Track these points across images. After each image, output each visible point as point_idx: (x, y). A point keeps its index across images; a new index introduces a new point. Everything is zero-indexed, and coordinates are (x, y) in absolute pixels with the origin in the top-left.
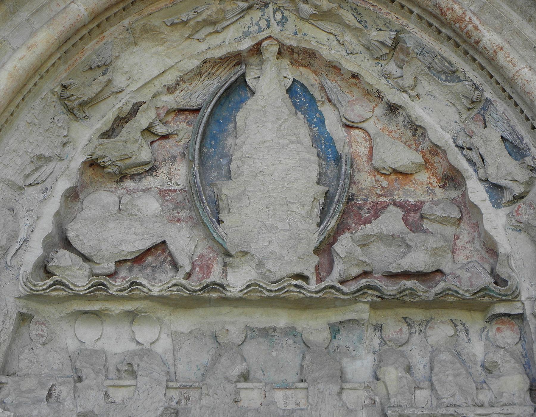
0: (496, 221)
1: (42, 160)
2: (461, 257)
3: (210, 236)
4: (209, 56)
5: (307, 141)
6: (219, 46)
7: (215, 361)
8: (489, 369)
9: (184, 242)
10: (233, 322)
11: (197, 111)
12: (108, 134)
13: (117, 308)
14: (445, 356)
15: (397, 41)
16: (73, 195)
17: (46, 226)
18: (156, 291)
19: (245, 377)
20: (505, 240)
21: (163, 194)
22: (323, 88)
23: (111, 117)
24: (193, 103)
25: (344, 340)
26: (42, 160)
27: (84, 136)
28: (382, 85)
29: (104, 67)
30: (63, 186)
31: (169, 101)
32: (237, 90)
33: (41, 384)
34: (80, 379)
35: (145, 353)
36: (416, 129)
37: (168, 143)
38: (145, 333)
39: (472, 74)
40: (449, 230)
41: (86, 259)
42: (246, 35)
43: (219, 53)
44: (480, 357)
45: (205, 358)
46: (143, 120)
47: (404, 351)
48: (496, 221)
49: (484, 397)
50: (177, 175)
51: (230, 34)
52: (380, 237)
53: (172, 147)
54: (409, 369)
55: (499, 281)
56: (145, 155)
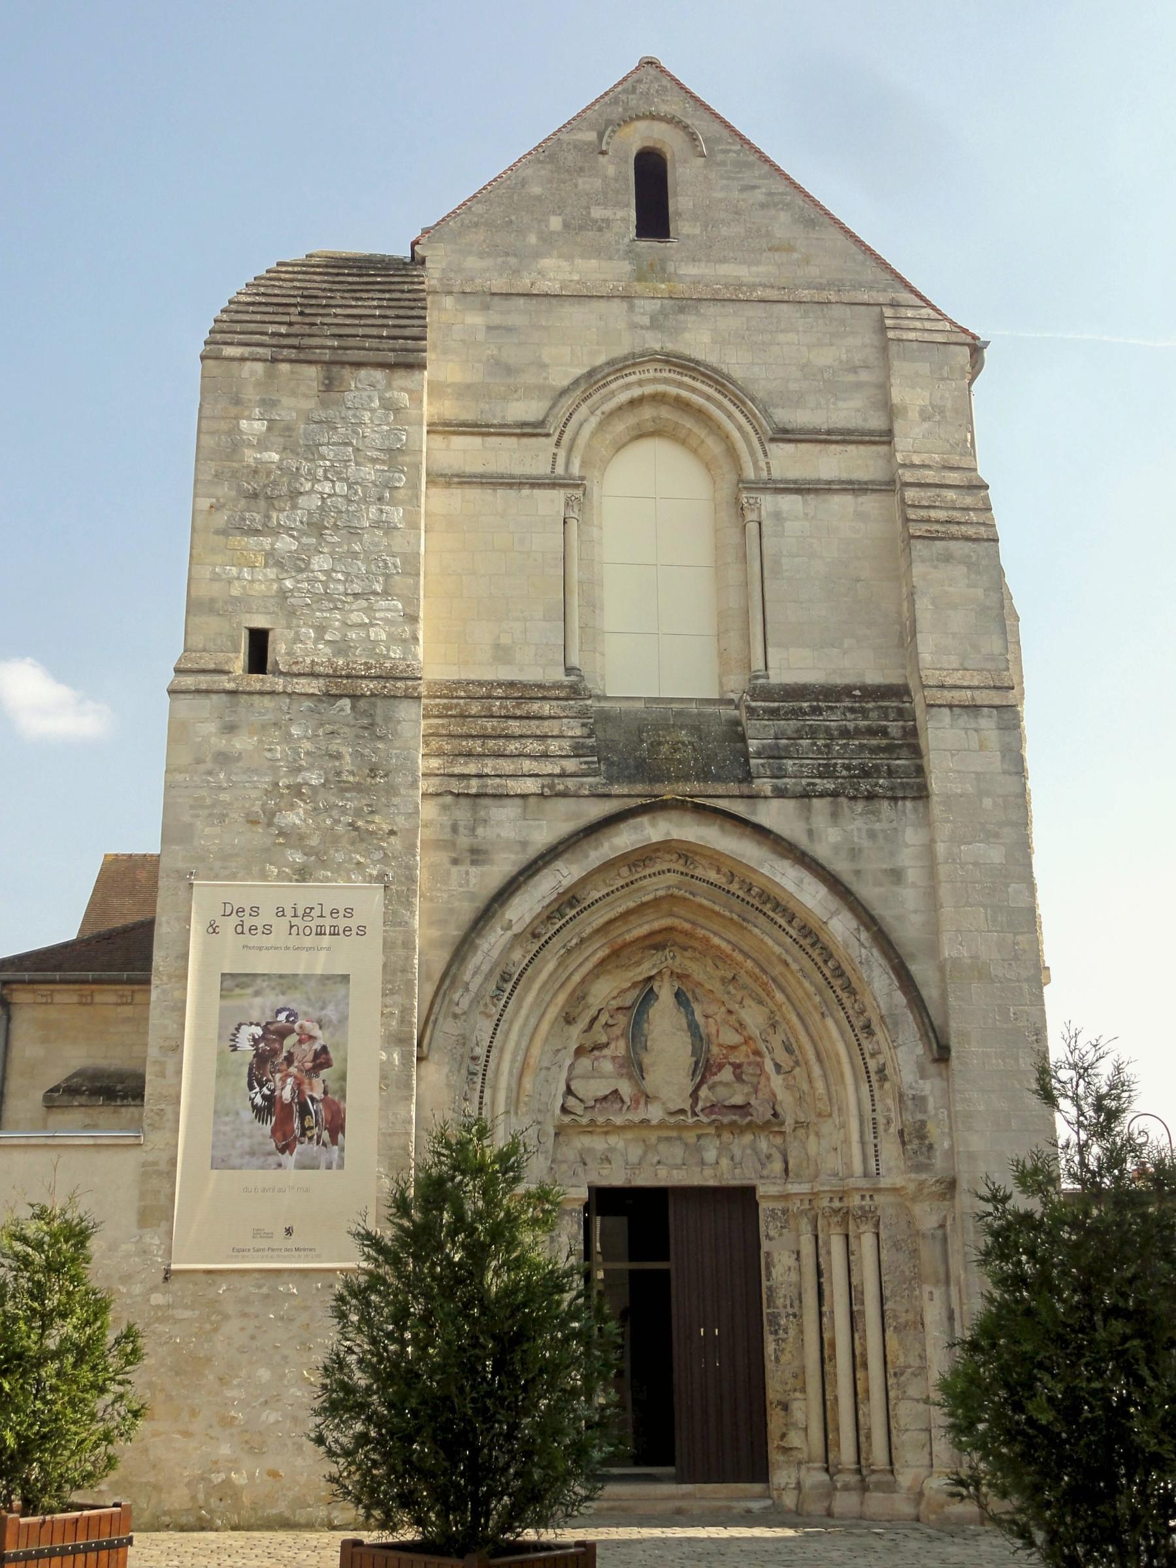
0: (777, 1082)
1: (558, 1051)
2: (760, 1094)
3: (637, 1084)
4: (635, 979)
5: (685, 1026)
6: (640, 974)
7: (645, 1153)
8: (769, 1157)
9: (626, 1089)
10: (653, 1137)
11: (629, 1008)
12: (585, 1031)
13: (599, 1130)
14: (749, 1151)
15: (734, 978)
16: (572, 1065)
17: (562, 1087)
18: (618, 1123)
19: (659, 1162)
20: (782, 1095)
21: (614, 1058)
22: (693, 992)
23: (588, 1020)
24: (628, 1003)
25: (702, 1142)
26: (558, 1051)
27: (575, 1032)
28: (726, 998)
29: (584, 998)
30: (568, 1062)
31: (615, 1004)
32: (648, 996)
33: (570, 1168)
34: (585, 1164)
35: (612, 1150)
36: (741, 1026)
37: (615, 1028)
38: (613, 1140)
39: (770, 1004)
40: (755, 1080)
41: (581, 1100)
42: (654, 966)
43: (641, 978)
44: (765, 1151)
45: (640, 1152)
46: (603, 1019)
47: (904, 812)
48: (777, 1082)
49: (765, 1173)
50: (619, 1048)
51: (646, 965)
52: (721, 1083)
53: (617, 1031)
54: (732, 1159)
55: (775, 1115)
56: (604, 1039)
